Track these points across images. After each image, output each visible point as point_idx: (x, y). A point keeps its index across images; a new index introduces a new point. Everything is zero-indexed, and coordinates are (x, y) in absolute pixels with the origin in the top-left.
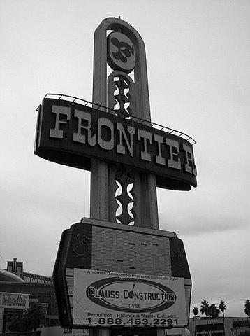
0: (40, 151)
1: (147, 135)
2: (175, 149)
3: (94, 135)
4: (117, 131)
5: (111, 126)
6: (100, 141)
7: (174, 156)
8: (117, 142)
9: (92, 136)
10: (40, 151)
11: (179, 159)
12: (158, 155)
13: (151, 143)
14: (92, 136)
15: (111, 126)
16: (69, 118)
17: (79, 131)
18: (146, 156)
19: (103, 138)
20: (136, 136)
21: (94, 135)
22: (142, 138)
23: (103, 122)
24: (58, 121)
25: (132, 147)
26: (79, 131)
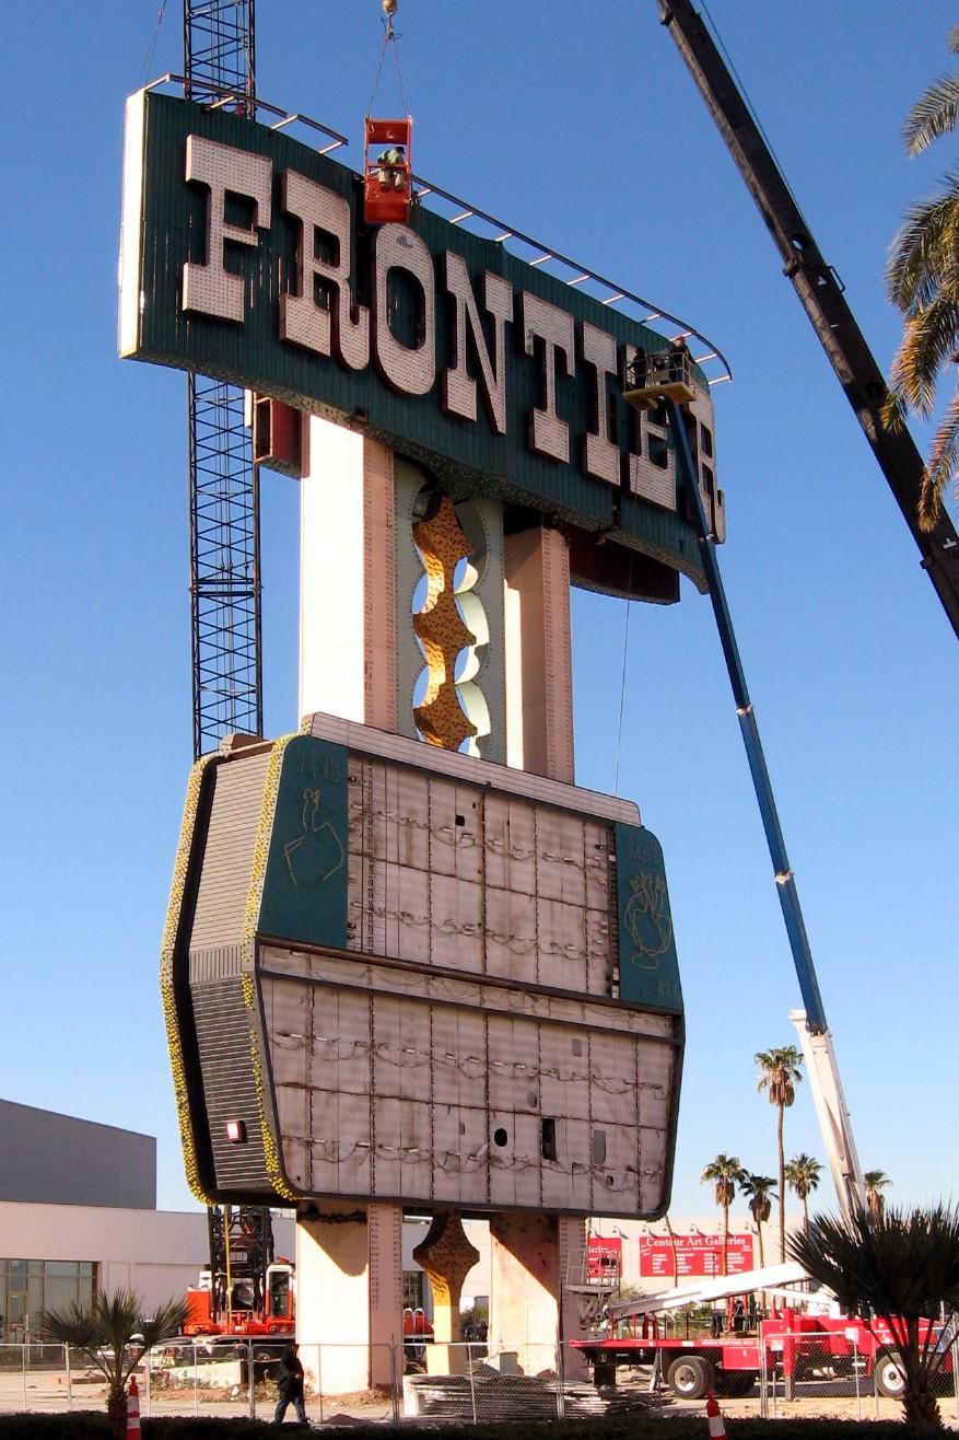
0: (155, 1139)
1: (248, 175)
2: (240, 207)
3: (364, 315)
4: (446, 301)
5: (425, 274)
6: (387, 347)
7: (230, 246)
8: (446, 360)
9: (354, 319)
10: (155, 1139)
11: (671, 459)
12: (543, 407)
13: (571, 370)
14: (354, 319)
15: (425, 274)
16: (264, 217)
17: (216, 253)
18: (551, 435)
19: (395, 333)
20: (516, 328)
21: (364, 315)
22: (539, 343)
23: (397, 248)
24: (220, 230)
25: (501, 383)
26: (216, 253)
